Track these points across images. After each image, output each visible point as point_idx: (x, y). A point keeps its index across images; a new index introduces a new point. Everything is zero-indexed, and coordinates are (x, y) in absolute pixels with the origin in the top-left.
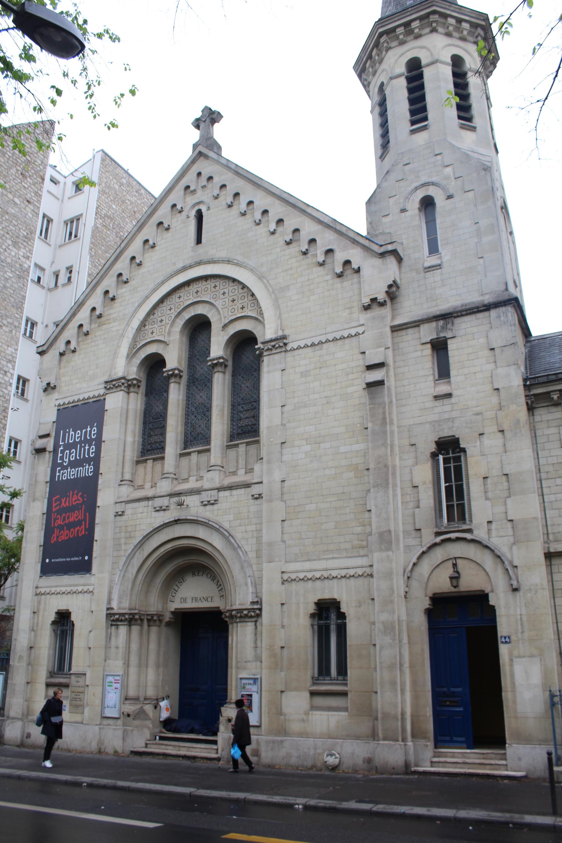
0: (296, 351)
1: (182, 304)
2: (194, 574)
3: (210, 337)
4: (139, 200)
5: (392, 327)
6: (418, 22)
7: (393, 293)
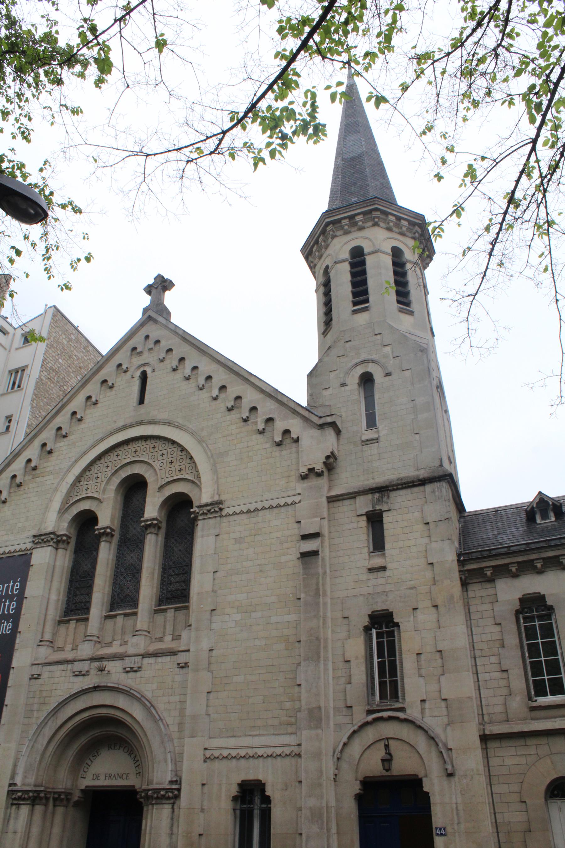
0: (231, 517)
2: (110, 748)
3: (145, 498)
4: (86, 356)
5: (328, 498)
6: (361, 216)
7: (330, 464)
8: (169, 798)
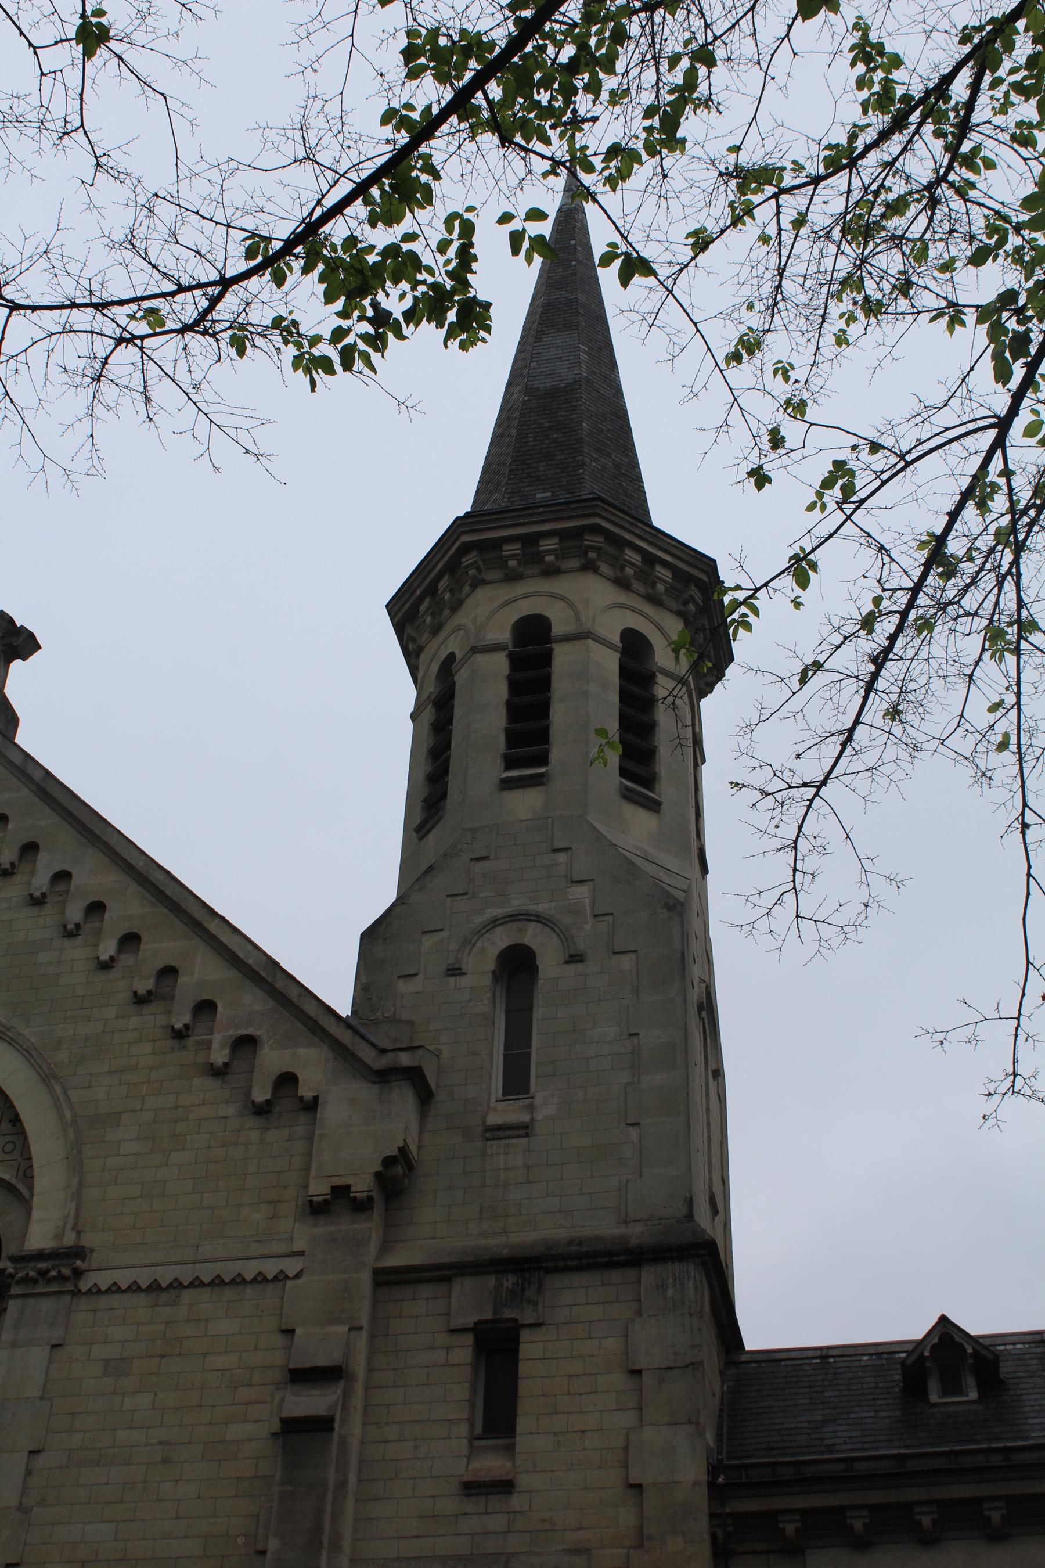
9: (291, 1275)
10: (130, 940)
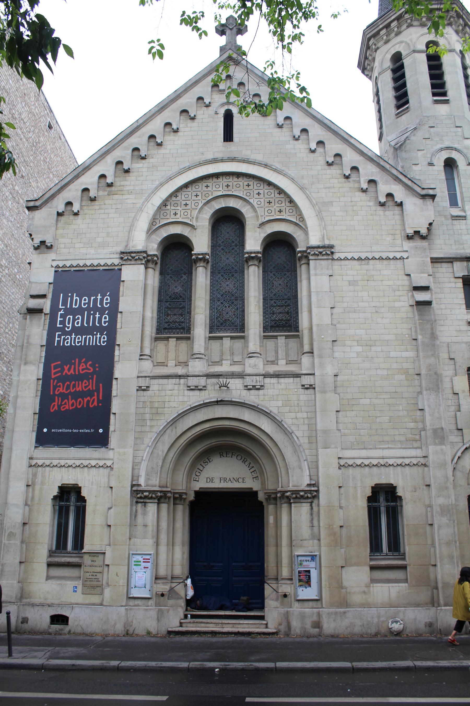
0: (343, 262)
1: (210, 193)
2: (221, 455)
5: (432, 258)
8: (308, 498)
9: (405, 258)
10: (320, 143)
